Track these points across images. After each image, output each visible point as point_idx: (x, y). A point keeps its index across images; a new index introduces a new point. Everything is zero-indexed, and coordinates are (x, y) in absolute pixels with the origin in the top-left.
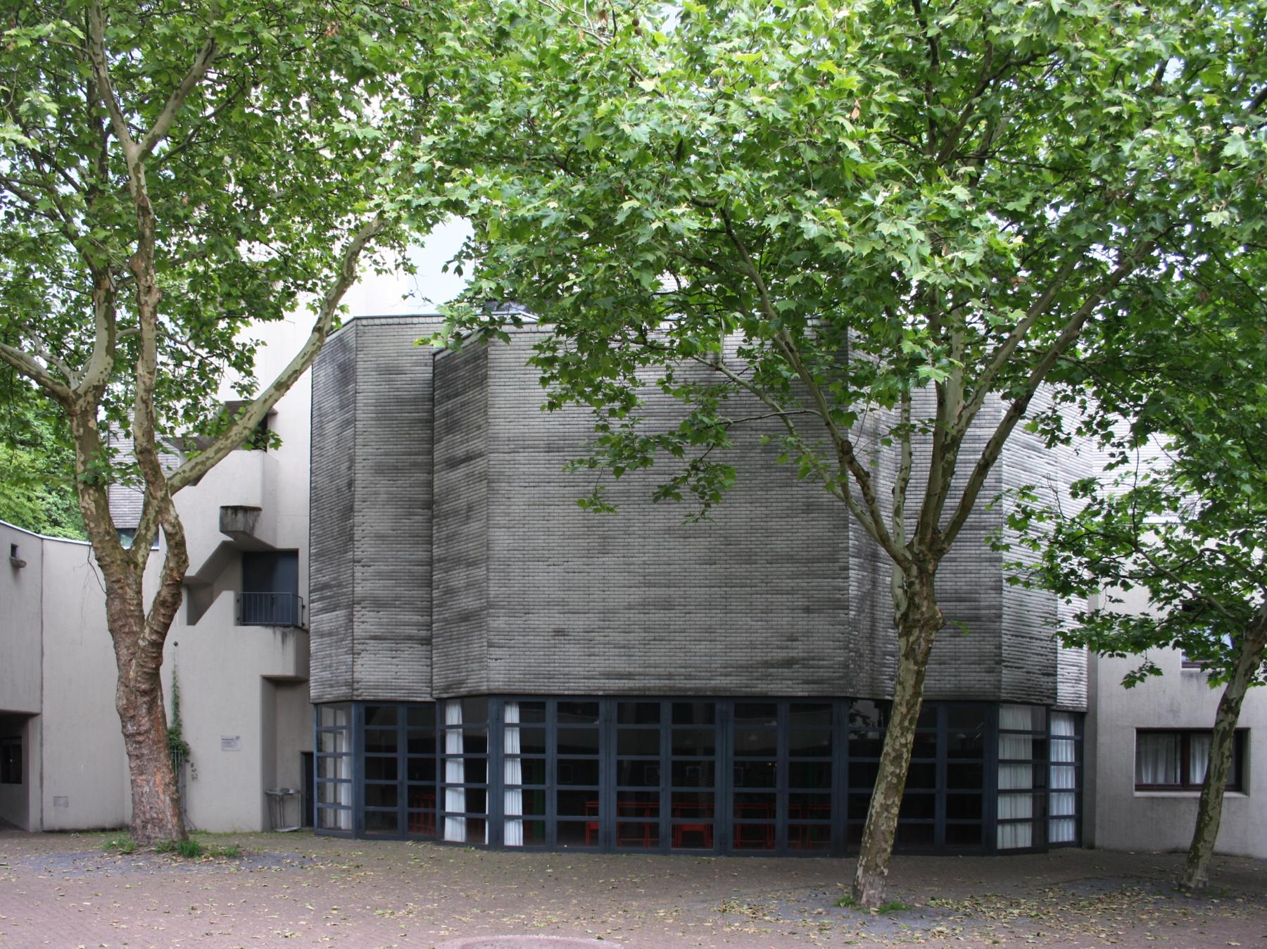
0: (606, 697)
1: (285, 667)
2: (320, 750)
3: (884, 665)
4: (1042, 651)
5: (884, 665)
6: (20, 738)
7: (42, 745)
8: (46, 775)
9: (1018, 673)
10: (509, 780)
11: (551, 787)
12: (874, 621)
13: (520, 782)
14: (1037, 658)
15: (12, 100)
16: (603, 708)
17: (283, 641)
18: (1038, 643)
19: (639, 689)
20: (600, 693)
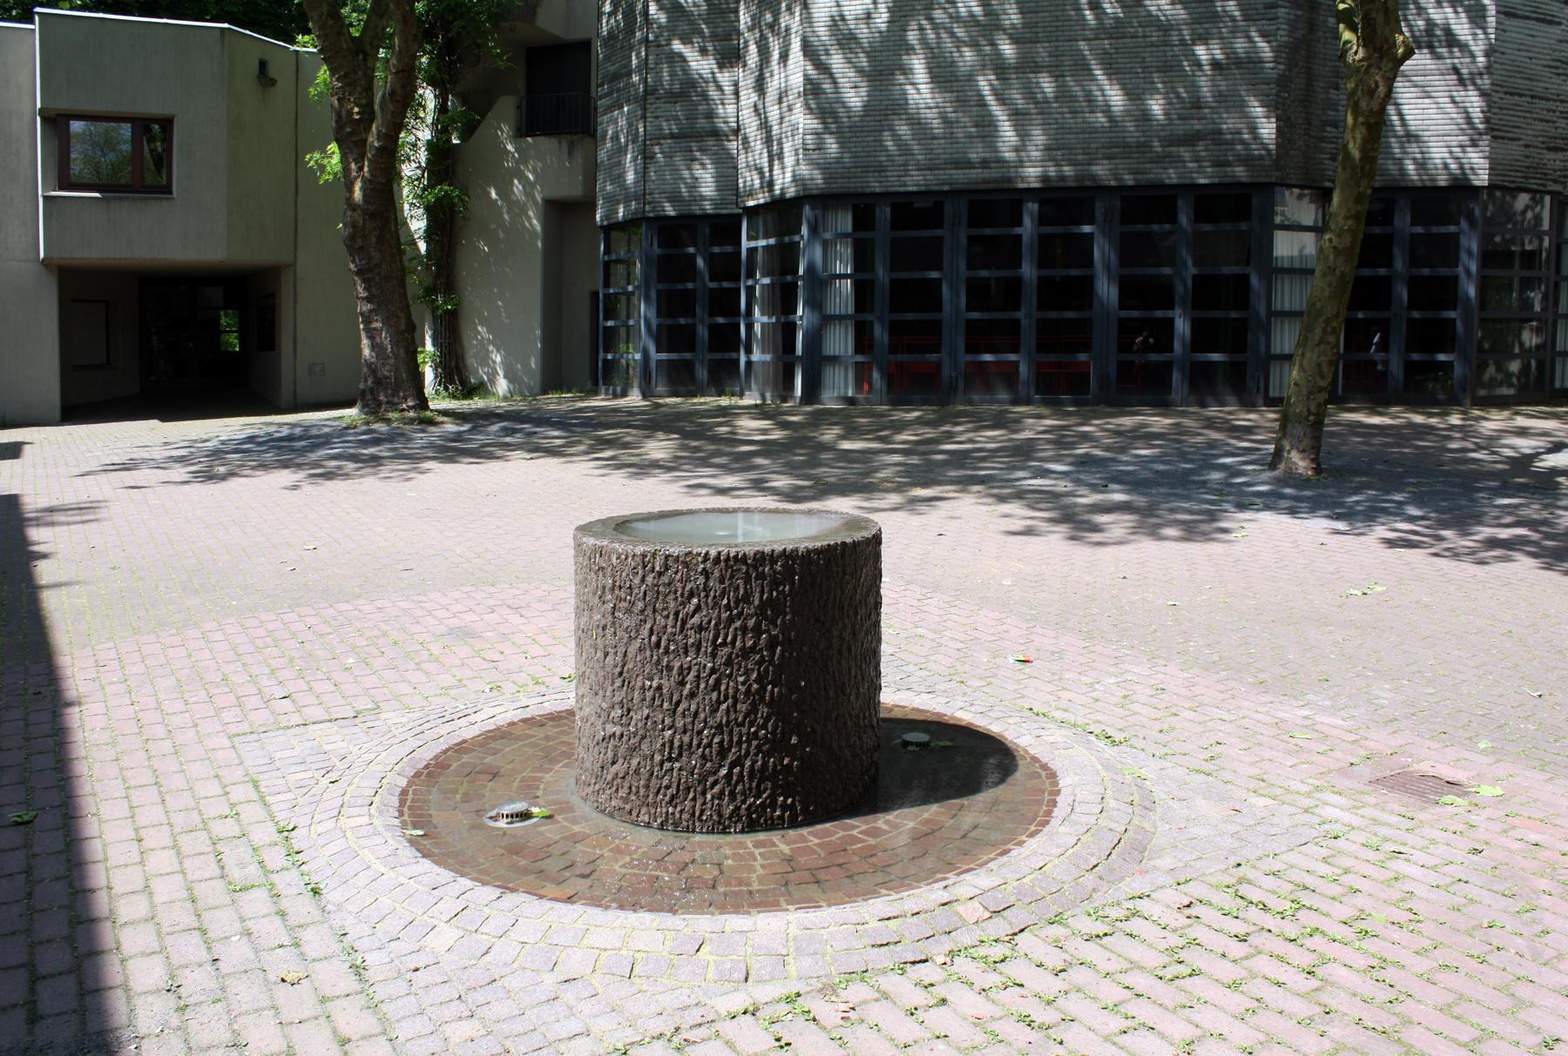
0: (956, 193)
1: (571, 189)
2: (607, 284)
3: (1323, 139)
4: (1549, 116)
5: (1323, 139)
6: (273, 295)
7: (295, 301)
8: (86, 526)
9: (1514, 146)
10: (839, 268)
11: (882, 273)
12: (1310, 78)
13: (850, 229)
14: (1540, 126)
15: (1562, 204)
16: (948, 209)
17: (570, 154)
18: (1543, 104)
19: (996, 181)
20: (946, 188)
